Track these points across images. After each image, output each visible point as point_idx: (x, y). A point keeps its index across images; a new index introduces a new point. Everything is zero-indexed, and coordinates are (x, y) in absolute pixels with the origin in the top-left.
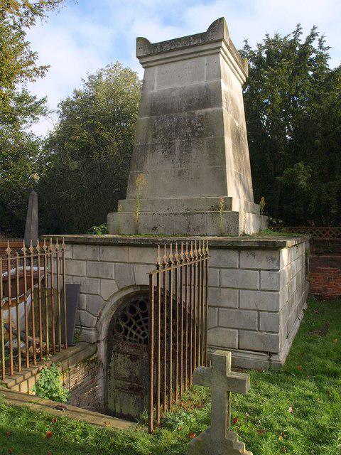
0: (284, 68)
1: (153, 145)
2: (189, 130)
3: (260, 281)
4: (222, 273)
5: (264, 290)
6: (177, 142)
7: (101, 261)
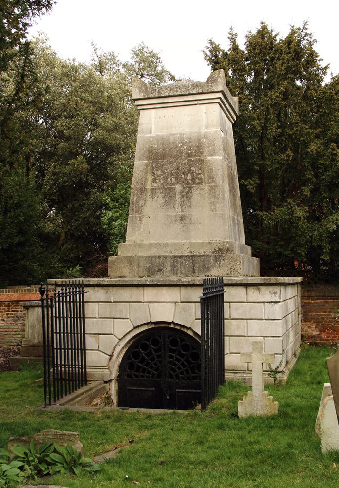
0: (267, 75)
1: (153, 189)
2: (189, 176)
3: (265, 311)
4: (232, 306)
5: (268, 319)
6: (178, 188)
7: (114, 302)
